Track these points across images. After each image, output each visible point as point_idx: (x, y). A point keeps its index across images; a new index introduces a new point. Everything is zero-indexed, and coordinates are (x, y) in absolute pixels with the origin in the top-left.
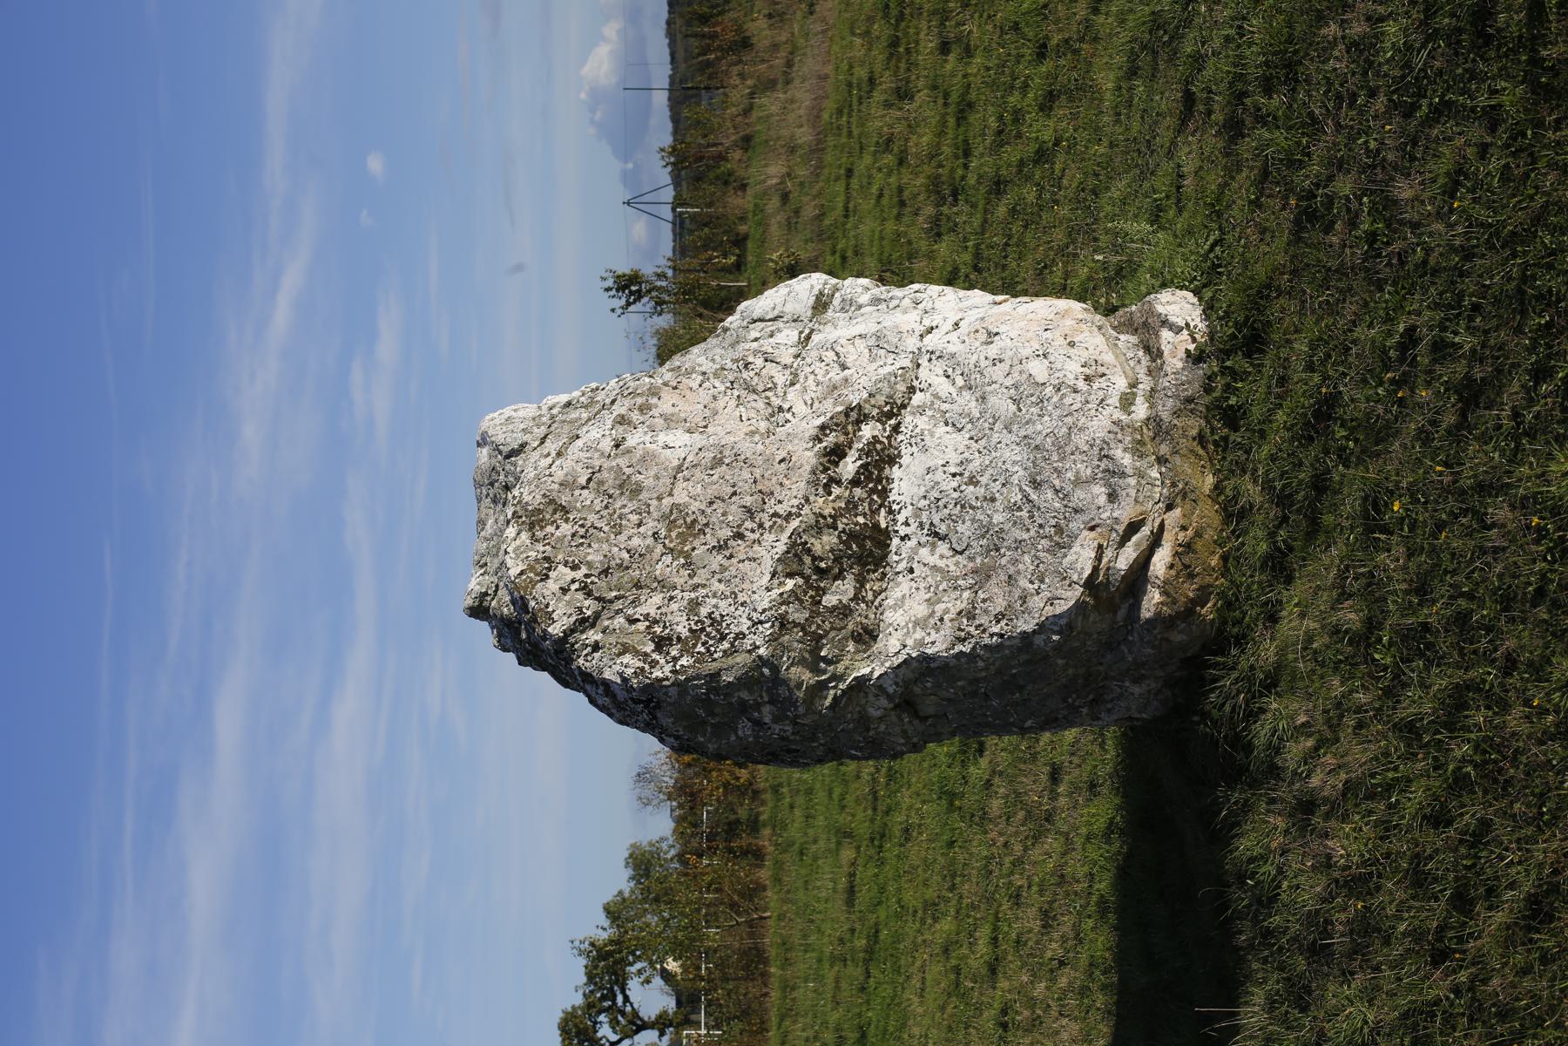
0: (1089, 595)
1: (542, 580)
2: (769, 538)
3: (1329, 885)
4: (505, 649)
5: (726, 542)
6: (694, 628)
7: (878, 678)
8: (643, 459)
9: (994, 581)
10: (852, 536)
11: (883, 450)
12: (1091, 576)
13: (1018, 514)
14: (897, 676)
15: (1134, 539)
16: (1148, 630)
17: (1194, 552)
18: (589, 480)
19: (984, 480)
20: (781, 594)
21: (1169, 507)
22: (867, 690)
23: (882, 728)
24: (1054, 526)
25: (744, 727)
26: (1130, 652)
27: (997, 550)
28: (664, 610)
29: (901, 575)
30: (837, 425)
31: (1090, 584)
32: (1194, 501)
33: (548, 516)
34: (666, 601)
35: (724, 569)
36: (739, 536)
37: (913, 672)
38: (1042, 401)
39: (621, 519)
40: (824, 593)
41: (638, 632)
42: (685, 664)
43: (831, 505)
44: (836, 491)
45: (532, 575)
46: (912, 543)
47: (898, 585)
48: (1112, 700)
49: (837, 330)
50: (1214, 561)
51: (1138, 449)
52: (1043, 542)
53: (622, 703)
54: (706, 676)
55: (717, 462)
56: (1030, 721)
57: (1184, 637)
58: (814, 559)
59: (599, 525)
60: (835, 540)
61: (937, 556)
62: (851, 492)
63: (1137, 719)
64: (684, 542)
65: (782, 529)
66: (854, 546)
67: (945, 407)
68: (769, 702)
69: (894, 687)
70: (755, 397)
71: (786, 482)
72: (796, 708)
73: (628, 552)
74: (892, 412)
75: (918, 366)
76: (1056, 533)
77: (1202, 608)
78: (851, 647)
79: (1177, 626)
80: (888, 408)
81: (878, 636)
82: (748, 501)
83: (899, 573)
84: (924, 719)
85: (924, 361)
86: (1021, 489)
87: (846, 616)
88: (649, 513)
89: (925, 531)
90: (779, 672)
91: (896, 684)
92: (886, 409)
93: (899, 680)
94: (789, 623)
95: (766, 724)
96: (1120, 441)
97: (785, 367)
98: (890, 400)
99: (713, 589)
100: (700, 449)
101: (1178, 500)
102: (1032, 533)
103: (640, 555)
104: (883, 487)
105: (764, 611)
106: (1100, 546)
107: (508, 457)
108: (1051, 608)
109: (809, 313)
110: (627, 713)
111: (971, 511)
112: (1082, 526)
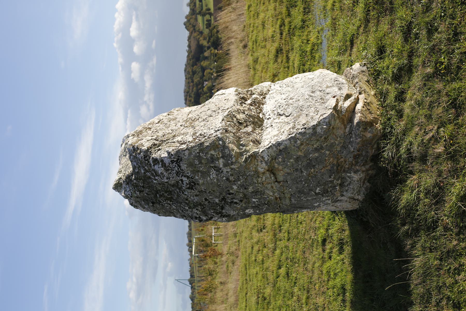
7: (262, 152)
14: (268, 152)
15: (349, 100)
16: (357, 129)
21: (360, 93)
25: (213, 173)
26: (352, 146)
31: (335, 108)
46: (272, 119)
56: (318, 189)
57: (371, 135)
67: (280, 91)
69: (268, 157)
72: (232, 158)
77: (376, 125)
83: (267, 128)
84: (279, 182)
89: (276, 115)
90: (225, 143)
93: (269, 154)
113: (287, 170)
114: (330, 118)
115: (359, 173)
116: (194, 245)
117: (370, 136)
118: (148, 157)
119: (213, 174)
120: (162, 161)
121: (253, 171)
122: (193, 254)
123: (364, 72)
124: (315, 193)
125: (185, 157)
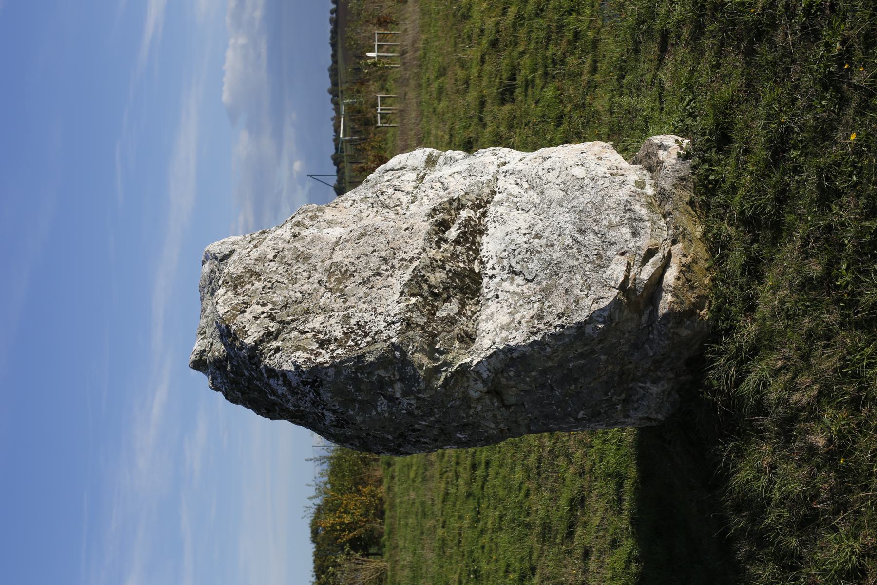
0: (623, 296)
1: (241, 313)
2: (399, 273)
3: (812, 470)
4: (217, 389)
5: (368, 279)
6: (346, 331)
7: (477, 365)
8: (312, 241)
9: (556, 293)
10: (456, 274)
11: (475, 225)
12: (623, 282)
13: (570, 251)
14: (489, 364)
15: (652, 260)
16: (664, 324)
17: (693, 272)
18: (275, 256)
19: (545, 235)
20: (407, 306)
21: (674, 242)
22: (469, 376)
23: (480, 408)
24: (596, 255)
25: (381, 404)
27: (557, 275)
28: (325, 324)
29: (490, 301)
30: (444, 209)
31: (623, 287)
32: (690, 241)
33: (246, 280)
34: (327, 319)
35: (367, 295)
36: (378, 274)
37: (500, 362)
38: (582, 187)
39: (296, 275)
40: (437, 310)
41: (307, 338)
42: (340, 353)
43: (441, 254)
44: (444, 246)
45: (234, 312)
46: (498, 279)
47: (488, 307)
48: (638, 401)
49: (442, 171)
50: (707, 281)
51: (650, 206)
52: (588, 265)
53: (295, 388)
54: (355, 358)
55: (363, 235)
56: (582, 412)
57: (689, 332)
58: (430, 286)
59: (281, 281)
60: (444, 276)
61: (515, 286)
62: (454, 247)
63: (655, 420)
64: (339, 284)
65: (407, 267)
66: (457, 281)
67: (516, 200)
68: (399, 380)
69: (488, 372)
70: (388, 210)
71: (409, 240)
72: (419, 383)
73: (301, 293)
74: (481, 205)
75: (497, 180)
76: (597, 259)
77: (701, 311)
78: (457, 344)
79: (684, 323)
80: (478, 202)
81: (475, 339)
82: (384, 254)
83: (489, 299)
84: (508, 407)
85: (501, 177)
86: (571, 236)
87: (453, 324)
88: (315, 270)
89: (506, 271)
90: (406, 355)
91: (489, 370)
92: (476, 203)
93: (491, 368)
94: (413, 323)
95: (397, 399)
96: (638, 201)
97: (408, 193)
98: (479, 197)
99: (360, 307)
100: (351, 231)
101: (680, 238)
102: (581, 261)
103: (309, 294)
104: (476, 247)
105: (395, 315)
106: (629, 264)
107: (222, 260)
108: (597, 305)
109: (423, 165)
110: (299, 396)
111: (537, 254)
112: (615, 253)
113: (523, 386)
114: (612, 310)
115: (662, 382)
116: (342, 120)
117: (688, 335)
118: (256, 359)
119: (382, 405)
120: (284, 374)
121: (459, 398)
122: (341, 136)
123: (685, 179)
124: (576, 419)
125: (328, 379)
